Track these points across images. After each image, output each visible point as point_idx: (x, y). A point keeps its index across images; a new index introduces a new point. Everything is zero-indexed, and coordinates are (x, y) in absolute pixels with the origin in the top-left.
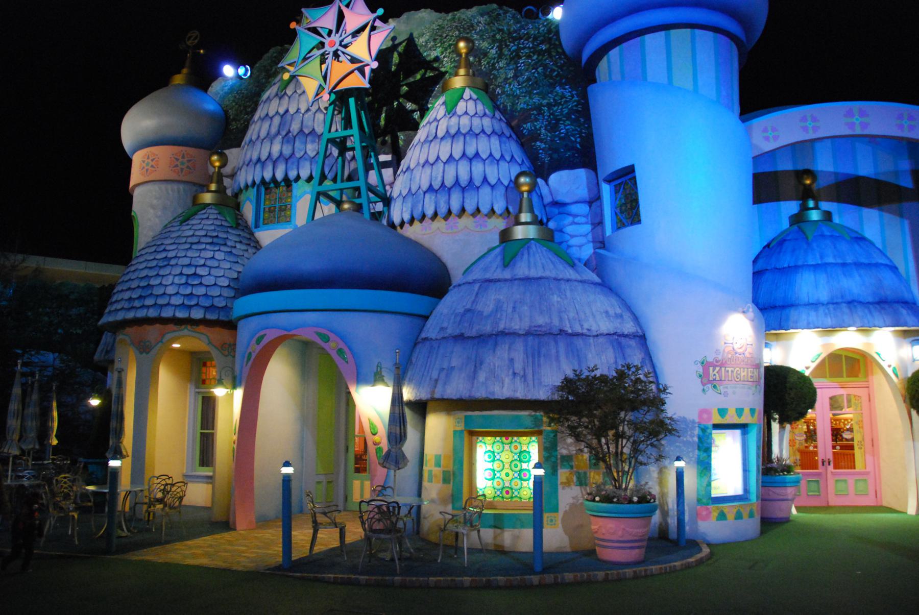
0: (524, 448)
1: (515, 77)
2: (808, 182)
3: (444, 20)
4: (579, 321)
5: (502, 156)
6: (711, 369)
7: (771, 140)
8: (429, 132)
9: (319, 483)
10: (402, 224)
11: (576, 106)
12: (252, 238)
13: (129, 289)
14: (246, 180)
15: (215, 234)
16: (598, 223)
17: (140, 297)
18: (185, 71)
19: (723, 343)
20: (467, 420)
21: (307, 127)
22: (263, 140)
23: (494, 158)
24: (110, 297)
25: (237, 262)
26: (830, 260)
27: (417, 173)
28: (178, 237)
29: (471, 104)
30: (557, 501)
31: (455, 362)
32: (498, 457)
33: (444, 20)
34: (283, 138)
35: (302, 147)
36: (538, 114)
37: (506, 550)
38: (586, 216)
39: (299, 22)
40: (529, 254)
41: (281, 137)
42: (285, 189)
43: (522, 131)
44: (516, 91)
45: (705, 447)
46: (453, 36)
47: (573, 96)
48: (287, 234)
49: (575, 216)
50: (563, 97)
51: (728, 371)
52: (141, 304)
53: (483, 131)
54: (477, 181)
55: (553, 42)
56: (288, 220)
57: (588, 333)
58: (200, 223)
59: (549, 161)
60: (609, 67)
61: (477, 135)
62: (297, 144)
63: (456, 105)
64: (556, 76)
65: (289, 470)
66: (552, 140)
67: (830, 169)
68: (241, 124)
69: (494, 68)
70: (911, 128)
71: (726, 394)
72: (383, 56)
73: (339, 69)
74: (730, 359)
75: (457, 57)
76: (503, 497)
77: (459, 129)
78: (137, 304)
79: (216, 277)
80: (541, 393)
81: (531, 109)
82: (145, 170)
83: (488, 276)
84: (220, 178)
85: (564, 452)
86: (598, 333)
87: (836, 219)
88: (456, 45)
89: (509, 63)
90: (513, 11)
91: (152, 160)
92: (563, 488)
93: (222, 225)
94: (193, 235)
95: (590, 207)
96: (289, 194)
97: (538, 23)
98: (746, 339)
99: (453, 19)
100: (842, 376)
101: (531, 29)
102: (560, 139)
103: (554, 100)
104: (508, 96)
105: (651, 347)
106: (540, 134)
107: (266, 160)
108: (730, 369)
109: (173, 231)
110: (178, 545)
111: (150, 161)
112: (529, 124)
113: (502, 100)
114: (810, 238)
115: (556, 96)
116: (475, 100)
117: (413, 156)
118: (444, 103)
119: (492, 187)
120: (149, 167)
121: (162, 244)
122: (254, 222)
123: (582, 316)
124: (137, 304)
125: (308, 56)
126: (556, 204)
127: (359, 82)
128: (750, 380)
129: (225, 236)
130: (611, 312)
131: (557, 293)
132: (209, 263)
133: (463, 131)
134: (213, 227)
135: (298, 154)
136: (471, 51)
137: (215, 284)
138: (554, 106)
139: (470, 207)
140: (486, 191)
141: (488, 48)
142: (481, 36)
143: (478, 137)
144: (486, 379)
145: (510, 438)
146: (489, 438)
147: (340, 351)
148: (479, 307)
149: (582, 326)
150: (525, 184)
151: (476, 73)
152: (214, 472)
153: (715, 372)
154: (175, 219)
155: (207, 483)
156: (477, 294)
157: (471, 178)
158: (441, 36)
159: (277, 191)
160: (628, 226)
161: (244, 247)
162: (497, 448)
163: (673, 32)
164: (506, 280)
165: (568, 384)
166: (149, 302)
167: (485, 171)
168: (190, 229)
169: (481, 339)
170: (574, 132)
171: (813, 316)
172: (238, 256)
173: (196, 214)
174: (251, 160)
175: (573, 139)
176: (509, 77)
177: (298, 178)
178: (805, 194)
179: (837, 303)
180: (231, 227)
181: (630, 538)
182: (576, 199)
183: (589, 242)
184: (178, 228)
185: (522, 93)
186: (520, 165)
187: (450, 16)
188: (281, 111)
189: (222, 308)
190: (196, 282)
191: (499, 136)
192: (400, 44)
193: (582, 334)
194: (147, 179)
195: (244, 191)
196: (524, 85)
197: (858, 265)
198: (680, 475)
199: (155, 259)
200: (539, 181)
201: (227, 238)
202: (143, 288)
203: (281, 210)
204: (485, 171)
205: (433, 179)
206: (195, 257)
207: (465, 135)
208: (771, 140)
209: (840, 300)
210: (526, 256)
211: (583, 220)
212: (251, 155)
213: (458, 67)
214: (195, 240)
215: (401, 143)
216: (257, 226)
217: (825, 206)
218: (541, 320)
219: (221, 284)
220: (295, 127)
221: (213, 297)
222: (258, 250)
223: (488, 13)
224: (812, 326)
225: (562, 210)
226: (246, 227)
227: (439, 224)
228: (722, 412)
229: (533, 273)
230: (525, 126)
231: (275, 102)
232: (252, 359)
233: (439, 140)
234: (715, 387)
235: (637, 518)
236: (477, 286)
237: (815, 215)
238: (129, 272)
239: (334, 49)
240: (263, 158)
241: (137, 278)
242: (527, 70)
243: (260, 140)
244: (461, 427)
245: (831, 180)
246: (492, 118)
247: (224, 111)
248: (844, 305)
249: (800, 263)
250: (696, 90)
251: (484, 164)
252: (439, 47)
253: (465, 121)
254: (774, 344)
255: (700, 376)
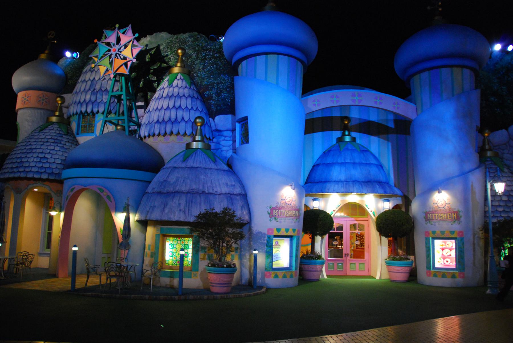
0: (186, 243)
1: (203, 69)
2: (346, 122)
3: (173, 38)
4: (212, 187)
5: (192, 108)
6: (274, 210)
7: (317, 105)
8: (159, 94)
9: (103, 258)
10: (145, 137)
11: (230, 85)
12: (75, 140)
13: (12, 163)
14: (73, 112)
15: (56, 138)
16: (234, 141)
17: (17, 167)
18: (47, 52)
19: (280, 199)
20: (161, 230)
21: (104, 87)
22: (82, 92)
23: (188, 108)
24: (2, 166)
25: (66, 152)
26: (348, 161)
27: (153, 114)
28: (37, 138)
29: (180, 82)
30: (198, 266)
31: (156, 204)
32: (175, 246)
33: (173, 38)
34: (92, 92)
35: (100, 97)
36: (212, 88)
37: (175, 287)
38: (230, 137)
39: (99, 40)
40: (195, 155)
41: (91, 91)
42: (92, 116)
43: (205, 95)
44: (203, 76)
45: (270, 246)
46: (176, 46)
47: (228, 80)
48: (92, 139)
49: (226, 137)
50: (224, 79)
51: (282, 212)
52: (17, 170)
53: (184, 95)
54: (179, 119)
55: (221, 53)
56: (93, 131)
57: (216, 193)
58: (49, 132)
59: (216, 110)
60: (242, 69)
61: (181, 97)
62: (98, 95)
63: (173, 82)
64: (222, 70)
65: (76, 249)
66: (218, 100)
67: (357, 116)
68: (74, 82)
69: (194, 64)
70: (380, 103)
71: (281, 222)
72: (140, 56)
73: (118, 62)
74: (283, 206)
75: (177, 57)
76: (176, 264)
77: (173, 93)
78: (15, 170)
79: (55, 159)
80: (191, 219)
81: (210, 85)
82: (23, 102)
83: (175, 165)
84: (61, 107)
85: (202, 245)
86: (221, 193)
87: (358, 141)
88: (177, 51)
89: (201, 62)
90: (205, 37)
91: (28, 97)
92: (201, 261)
93: (60, 133)
94: (45, 138)
95: (232, 133)
96: (94, 119)
97: (216, 43)
98: (292, 198)
99: (177, 38)
100: (356, 215)
101: (212, 46)
102: (222, 100)
103: (220, 81)
104: (199, 77)
105: (249, 200)
106: (212, 97)
107: (83, 102)
108: (283, 211)
109: (35, 135)
110: (27, 283)
111: (26, 97)
112: (208, 92)
113: (197, 79)
114: (341, 150)
115: (222, 79)
116: (182, 80)
117: (153, 105)
118: (168, 80)
119: (186, 122)
120: (25, 101)
121: (29, 141)
122: (76, 132)
123: (214, 185)
124: (15, 170)
125: (106, 53)
126: (218, 131)
127: (124, 71)
128: (293, 216)
129: (60, 139)
130: (229, 183)
131: (204, 174)
132: (51, 152)
133: (175, 95)
134: (55, 134)
135: (99, 101)
136: (184, 54)
137: (54, 162)
138: (220, 84)
139: (175, 131)
140: (183, 124)
141: (192, 54)
142: (189, 47)
143: (182, 98)
144: (168, 212)
145: (180, 238)
146: (172, 238)
147: (108, 197)
148: (169, 180)
149: (213, 190)
150: (199, 122)
151: (186, 66)
152: (51, 251)
153: (276, 212)
154: (33, 131)
155: (48, 256)
156: (169, 173)
157: (176, 117)
158: (171, 46)
159: (88, 117)
160: (245, 144)
161: (70, 145)
162: (175, 242)
163: (269, 56)
164: (182, 168)
165: (201, 216)
166: (21, 170)
167: (183, 114)
168: (44, 135)
169: (168, 194)
170: (228, 97)
171: (336, 187)
172: (66, 149)
173: (47, 127)
174: (76, 102)
175: (227, 100)
176: (200, 68)
177: (98, 112)
178: (345, 128)
179: (348, 181)
180: (65, 134)
181: (224, 283)
182: (225, 129)
183: (231, 149)
184: (37, 134)
185: (206, 76)
186: (200, 112)
187: (175, 37)
188: (92, 78)
189: (57, 174)
190: (45, 161)
191: (192, 98)
192: (152, 49)
193: (213, 193)
194: (24, 107)
195: (72, 116)
196: (207, 73)
197: (360, 164)
198: (255, 257)
199: (25, 149)
200: (211, 119)
201: (62, 140)
202: (19, 162)
203: (89, 127)
204: (183, 114)
205: (159, 117)
206: (45, 149)
207: (175, 97)
208: (317, 105)
209: (350, 180)
210: (194, 157)
211: (229, 139)
212: (76, 100)
213: (177, 62)
214: (46, 140)
215: (149, 97)
216: (78, 134)
217: (353, 134)
218: (194, 187)
219: (57, 162)
220: (98, 87)
221: (53, 168)
222: (77, 145)
223: (193, 37)
224: (335, 192)
225: (219, 133)
226: (73, 134)
227: (161, 138)
228: (278, 230)
229: (195, 165)
230: (206, 93)
231: (89, 74)
232: (69, 199)
233: (164, 98)
234: (275, 219)
235: (223, 274)
236: (170, 169)
237: (347, 139)
238: (12, 154)
239: (115, 53)
240: (82, 101)
241: (16, 157)
242: (209, 66)
243: (81, 92)
244: (159, 233)
245: (358, 122)
246: (190, 89)
247: (65, 74)
248: (351, 182)
249: (335, 162)
250: (277, 84)
251: (183, 111)
252: (169, 51)
253: (176, 90)
254: (321, 199)
255: (269, 213)
